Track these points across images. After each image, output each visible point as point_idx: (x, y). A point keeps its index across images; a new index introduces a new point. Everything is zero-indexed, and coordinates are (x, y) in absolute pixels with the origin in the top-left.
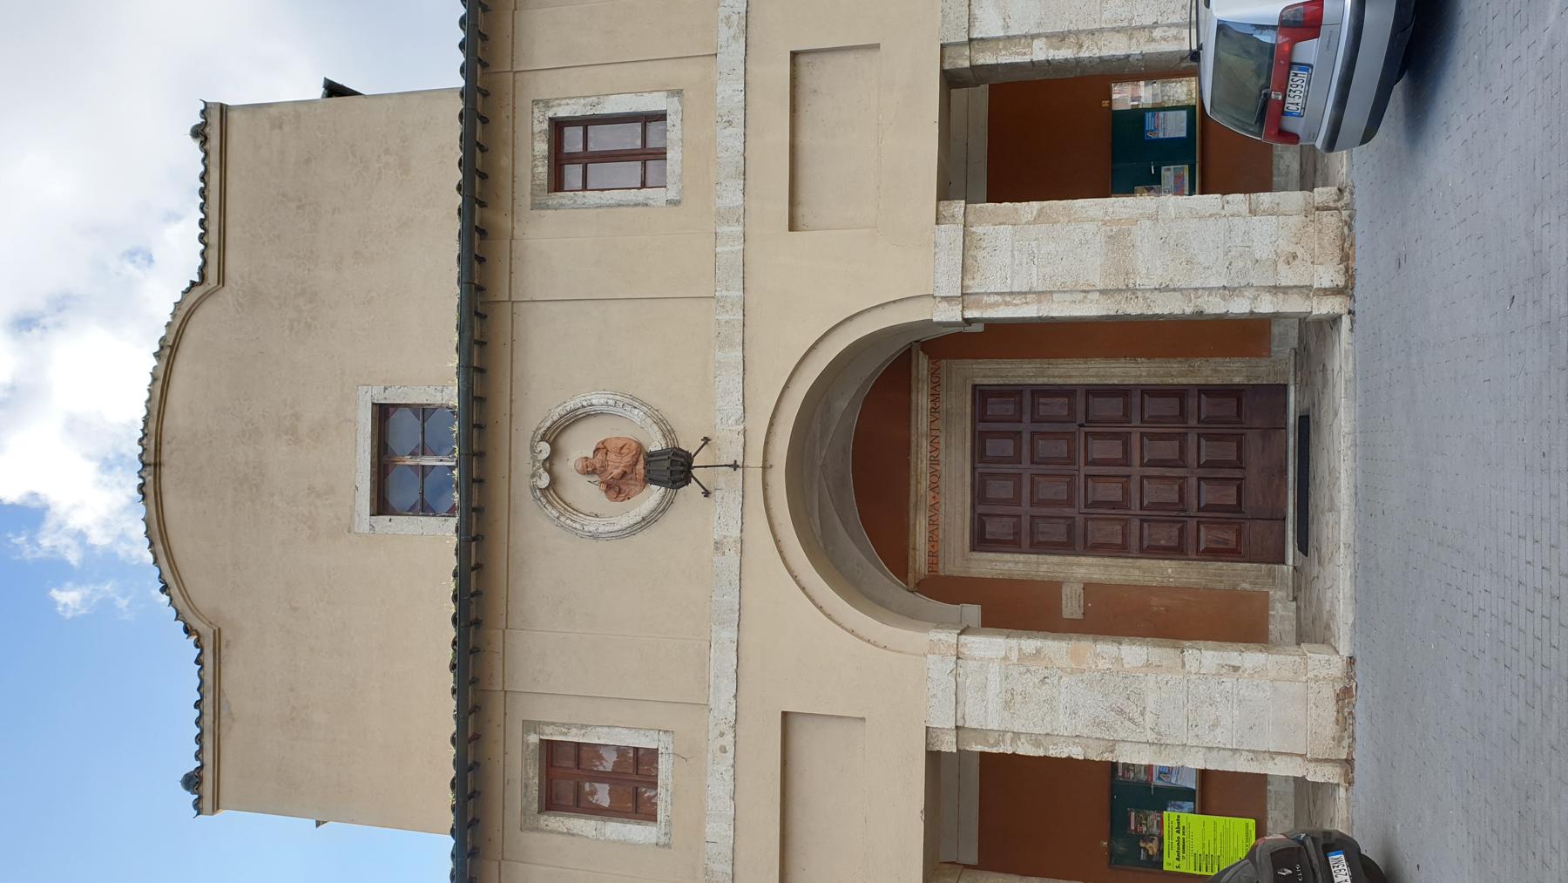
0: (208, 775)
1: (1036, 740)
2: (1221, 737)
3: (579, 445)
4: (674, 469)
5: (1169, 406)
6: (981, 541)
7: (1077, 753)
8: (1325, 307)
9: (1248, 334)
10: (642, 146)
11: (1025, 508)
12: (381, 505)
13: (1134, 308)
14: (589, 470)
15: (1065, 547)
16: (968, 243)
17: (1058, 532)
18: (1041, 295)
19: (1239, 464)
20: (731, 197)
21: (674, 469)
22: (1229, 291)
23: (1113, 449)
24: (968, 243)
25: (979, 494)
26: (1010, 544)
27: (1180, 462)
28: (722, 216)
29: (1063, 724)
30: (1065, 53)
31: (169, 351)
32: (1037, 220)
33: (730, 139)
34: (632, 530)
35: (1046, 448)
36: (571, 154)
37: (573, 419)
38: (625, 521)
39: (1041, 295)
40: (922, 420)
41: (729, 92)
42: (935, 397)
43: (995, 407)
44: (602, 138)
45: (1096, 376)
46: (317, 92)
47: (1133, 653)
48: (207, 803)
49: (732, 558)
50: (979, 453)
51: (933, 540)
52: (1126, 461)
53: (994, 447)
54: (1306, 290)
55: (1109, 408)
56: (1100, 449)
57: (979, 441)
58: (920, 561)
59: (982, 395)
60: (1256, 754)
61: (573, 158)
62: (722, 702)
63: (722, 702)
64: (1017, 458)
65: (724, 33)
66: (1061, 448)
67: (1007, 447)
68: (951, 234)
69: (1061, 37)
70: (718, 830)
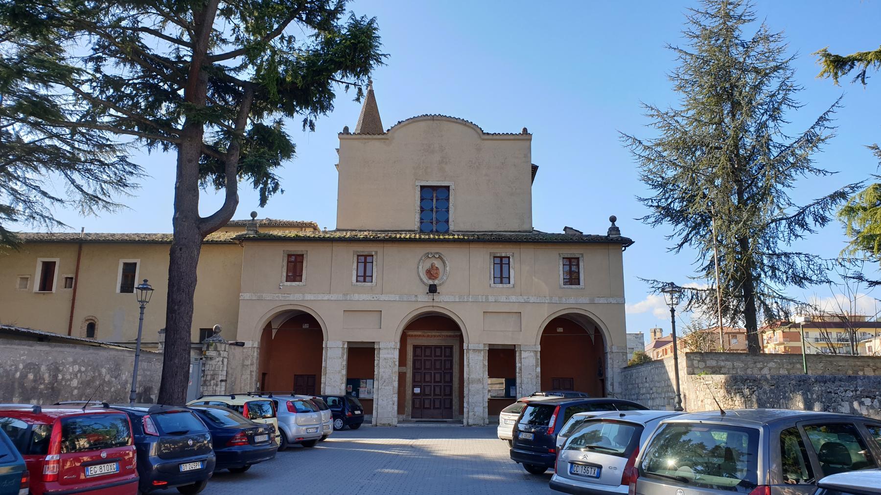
0: (349, 136)
1: (378, 364)
2: (380, 402)
3: (438, 264)
4: (433, 289)
5: (447, 392)
6: (415, 347)
7: (376, 373)
8: (465, 421)
9: (461, 412)
10: (502, 277)
11: (423, 358)
12: (422, 187)
13: (465, 384)
14: (432, 266)
15: (414, 368)
16: (479, 351)
17: (418, 366)
18: (468, 365)
19: (434, 408)
20: (491, 299)
21: (433, 289)
22: (468, 403)
23: (438, 379)
24: (479, 351)
25: (427, 347)
26: (415, 355)
27: (435, 395)
28: (487, 296)
29: (381, 370)
30: (518, 370)
31: (464, 123)
32: (484, 365)
33: (503, 299)
34: (419, 276)
35: (438, 363)
36: (502, 264)
37: (444, 262)
38: (421, 275)
39: (468, 365)
40: (445, 333)
41: (513, 299)
42: (450, 336)
43: (448, 350)
44: (505, 267)
45: (641, 414)
46: (534, 161)
47: (396, 384)
48: (342, 136)
49: (414, 299)
50: (436, 347)
51: (415, 336)
52: (435, 382)
53: (438, 350)
54: (468, 417)
55: (448, 378)
56: (438, 376)
57: (440, 347)
58: (410, 333)
59: (451, 348)
60: (377, 408)
61: (501, 261)
62: (383, 297)
63: (383, 297)
64: (436, 356)
65: (525, 297)
66: (438, 366)
67: (438, 353)
68: (481, 347)
69: (521, 370)
70: (356, 297)
